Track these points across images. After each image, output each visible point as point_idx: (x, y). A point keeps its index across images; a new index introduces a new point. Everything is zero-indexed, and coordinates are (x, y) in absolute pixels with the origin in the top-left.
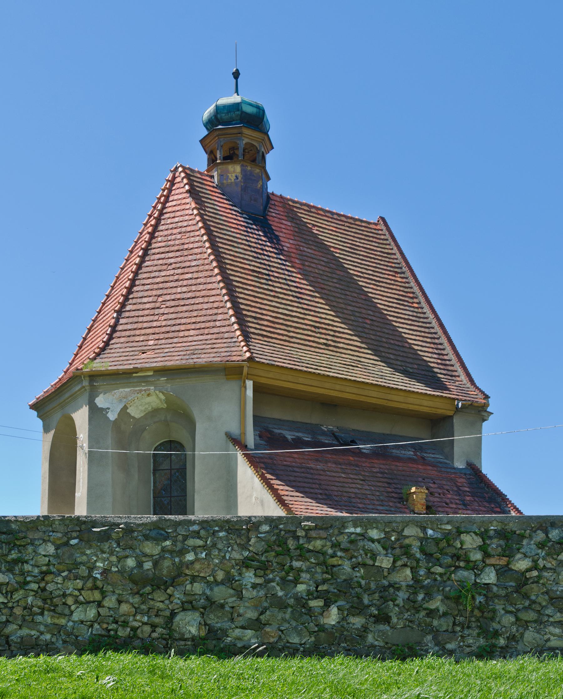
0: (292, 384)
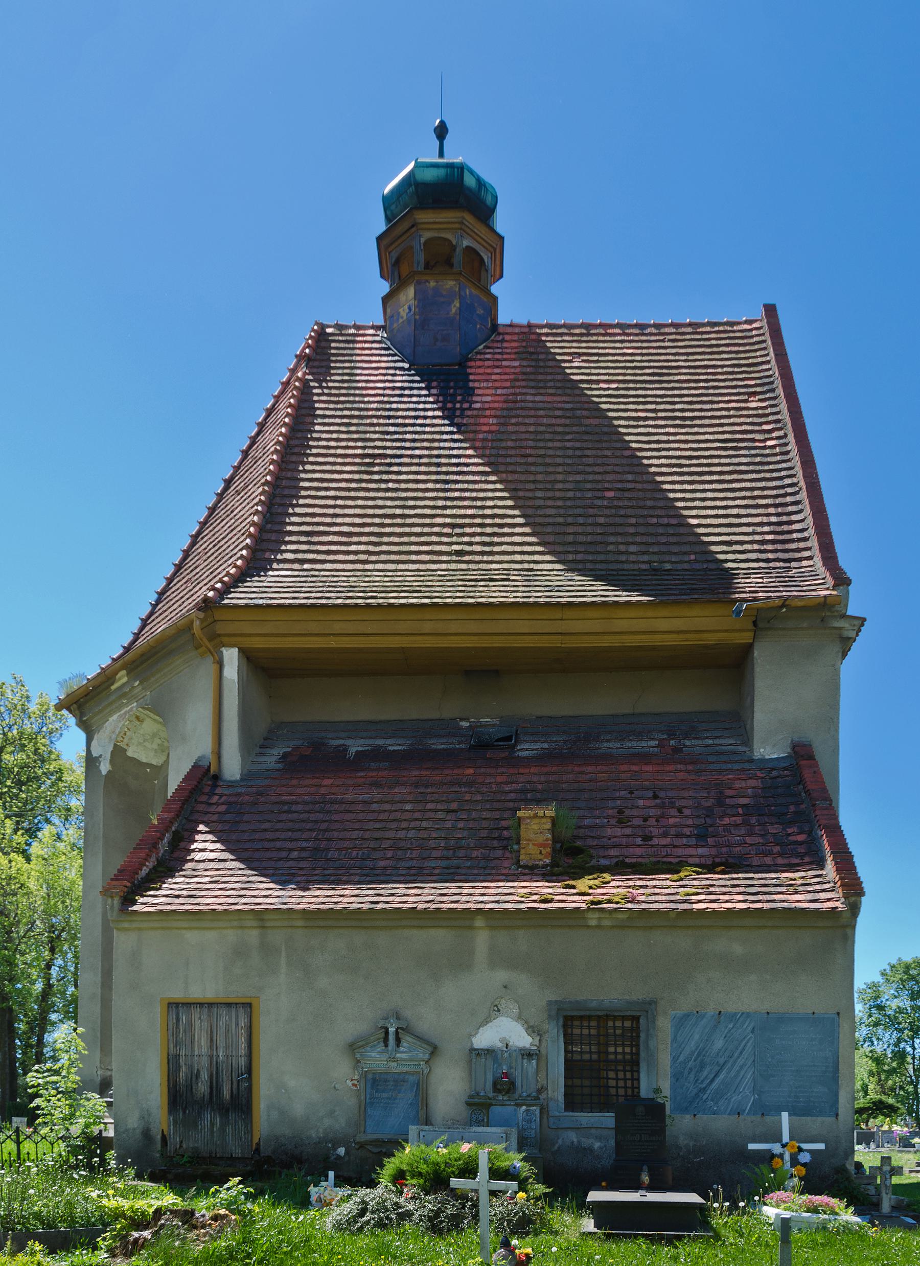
0: (320, 639)
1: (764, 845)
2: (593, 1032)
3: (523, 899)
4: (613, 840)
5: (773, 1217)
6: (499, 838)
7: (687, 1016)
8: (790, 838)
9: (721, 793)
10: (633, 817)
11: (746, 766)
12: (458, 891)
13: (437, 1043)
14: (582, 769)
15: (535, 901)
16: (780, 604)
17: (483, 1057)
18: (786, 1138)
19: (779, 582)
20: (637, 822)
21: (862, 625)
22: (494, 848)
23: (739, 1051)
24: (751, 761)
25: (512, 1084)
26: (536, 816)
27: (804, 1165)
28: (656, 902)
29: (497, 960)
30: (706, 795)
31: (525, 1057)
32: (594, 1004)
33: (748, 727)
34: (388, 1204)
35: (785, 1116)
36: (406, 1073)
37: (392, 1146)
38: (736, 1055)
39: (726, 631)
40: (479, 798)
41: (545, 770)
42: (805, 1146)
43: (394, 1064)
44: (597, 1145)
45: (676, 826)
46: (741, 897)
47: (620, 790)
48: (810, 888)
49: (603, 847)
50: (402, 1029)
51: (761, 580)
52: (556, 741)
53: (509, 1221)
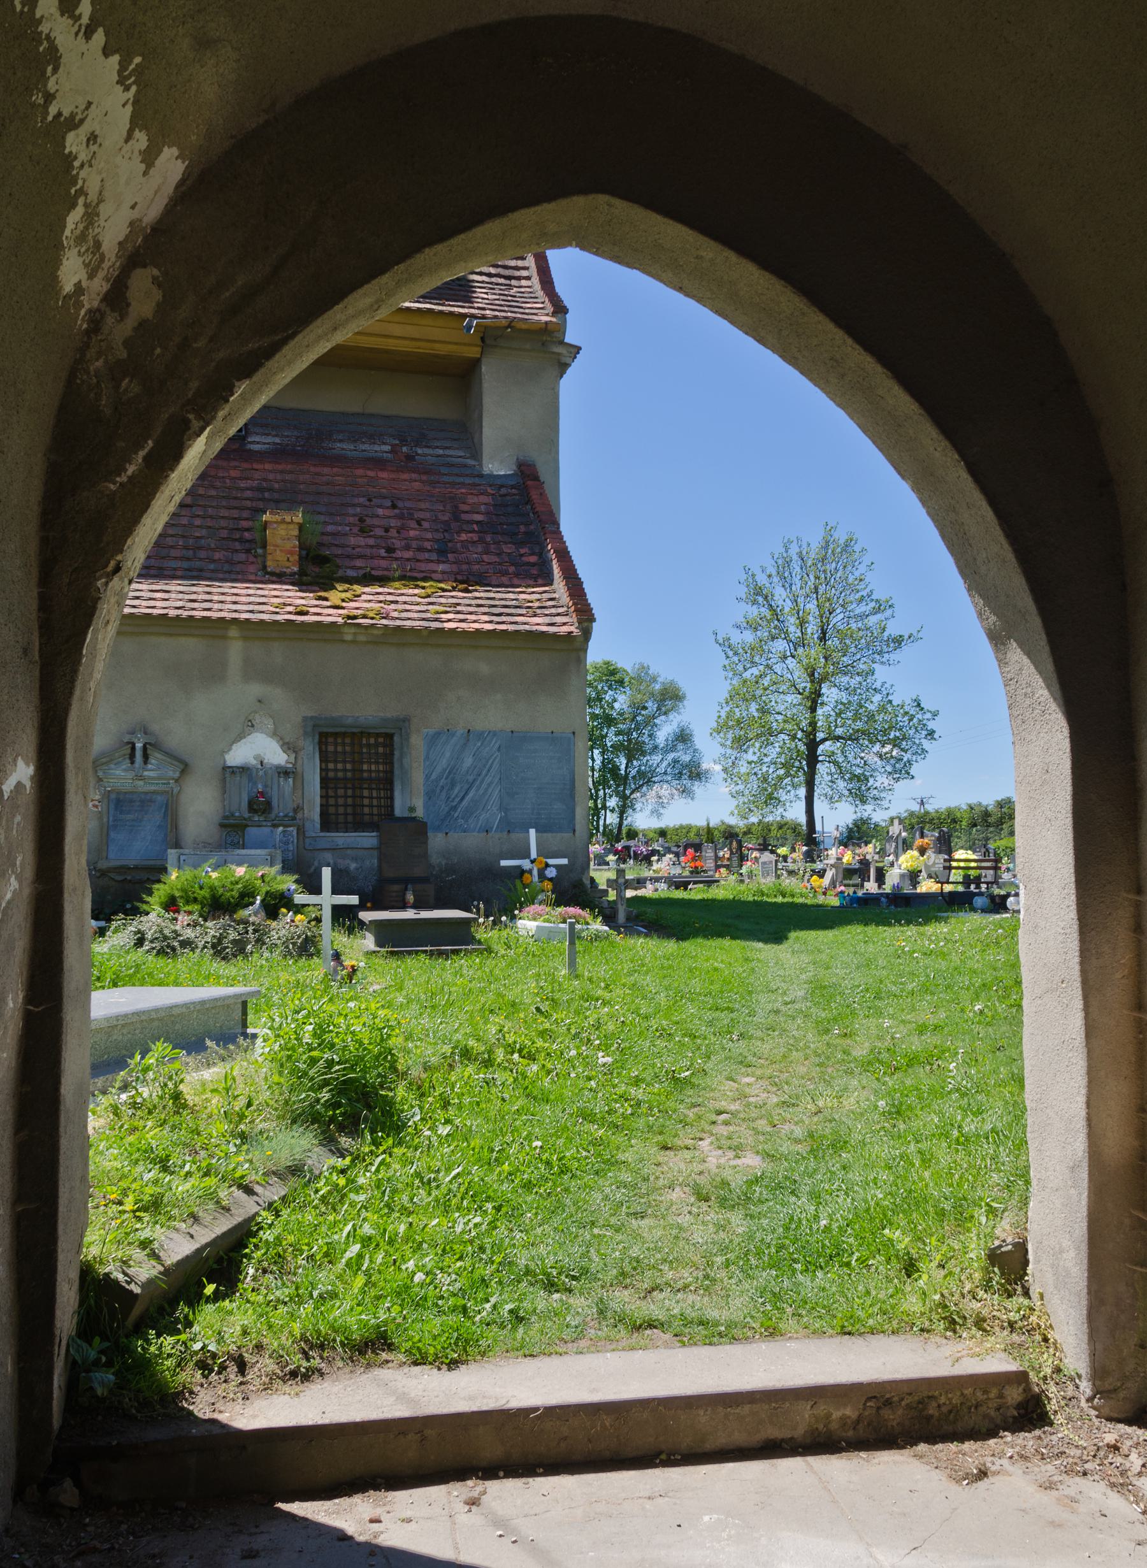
1: (500, 564)
2: (348, 749)
3: (277, 610)
4: (358, 550)
5: (534, 929)
6: (241, 540)
7: (438, 734)
8: (523, 559)
9: (456, 507)
10: (374, 526)
11: (477, 480)
12: (208, 597)
13: (187, 760)
14: (318, 470)
15: (290, 613)
16: (507, 324)
17: (238, 775)
18: (534, 855)
19: (503, 300)
20: (379, 532)
21: (578, 353)
22: (237, 551)
23: (486, 770)
24: (481, 476)
25: (268, 805)
26: (283, 521)
27: (551, 880)
28: (409, 619)
29: (251, 672)
30: (442, 508)
31: (282, 775)
32: (350, 721)
33: (476, 440)
34: (167, 932)
35: (532, 832)
36: (154, 792)
37: (158, 872)
38: (484, 773)
39: (456, 344)
40: (213, 493)
41: (280, 467)
42: (551, 861)
43: (141, 783)
44: (353, 866)
45: (417, 539)
46: (486, 618)
47: (358, 496)
48: (547, 612)
49: (348, 557)
50: (150, 744)
51: (485, 296)
52: (288, 436)
53: (294, 944)
